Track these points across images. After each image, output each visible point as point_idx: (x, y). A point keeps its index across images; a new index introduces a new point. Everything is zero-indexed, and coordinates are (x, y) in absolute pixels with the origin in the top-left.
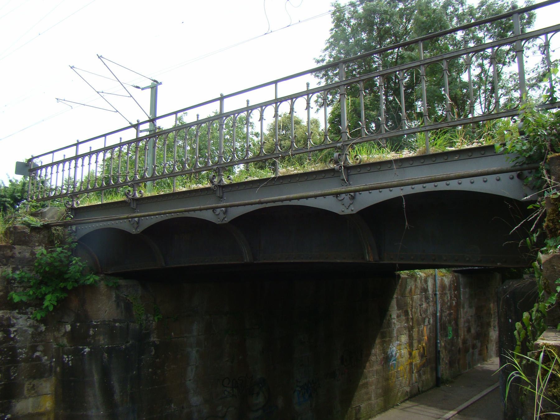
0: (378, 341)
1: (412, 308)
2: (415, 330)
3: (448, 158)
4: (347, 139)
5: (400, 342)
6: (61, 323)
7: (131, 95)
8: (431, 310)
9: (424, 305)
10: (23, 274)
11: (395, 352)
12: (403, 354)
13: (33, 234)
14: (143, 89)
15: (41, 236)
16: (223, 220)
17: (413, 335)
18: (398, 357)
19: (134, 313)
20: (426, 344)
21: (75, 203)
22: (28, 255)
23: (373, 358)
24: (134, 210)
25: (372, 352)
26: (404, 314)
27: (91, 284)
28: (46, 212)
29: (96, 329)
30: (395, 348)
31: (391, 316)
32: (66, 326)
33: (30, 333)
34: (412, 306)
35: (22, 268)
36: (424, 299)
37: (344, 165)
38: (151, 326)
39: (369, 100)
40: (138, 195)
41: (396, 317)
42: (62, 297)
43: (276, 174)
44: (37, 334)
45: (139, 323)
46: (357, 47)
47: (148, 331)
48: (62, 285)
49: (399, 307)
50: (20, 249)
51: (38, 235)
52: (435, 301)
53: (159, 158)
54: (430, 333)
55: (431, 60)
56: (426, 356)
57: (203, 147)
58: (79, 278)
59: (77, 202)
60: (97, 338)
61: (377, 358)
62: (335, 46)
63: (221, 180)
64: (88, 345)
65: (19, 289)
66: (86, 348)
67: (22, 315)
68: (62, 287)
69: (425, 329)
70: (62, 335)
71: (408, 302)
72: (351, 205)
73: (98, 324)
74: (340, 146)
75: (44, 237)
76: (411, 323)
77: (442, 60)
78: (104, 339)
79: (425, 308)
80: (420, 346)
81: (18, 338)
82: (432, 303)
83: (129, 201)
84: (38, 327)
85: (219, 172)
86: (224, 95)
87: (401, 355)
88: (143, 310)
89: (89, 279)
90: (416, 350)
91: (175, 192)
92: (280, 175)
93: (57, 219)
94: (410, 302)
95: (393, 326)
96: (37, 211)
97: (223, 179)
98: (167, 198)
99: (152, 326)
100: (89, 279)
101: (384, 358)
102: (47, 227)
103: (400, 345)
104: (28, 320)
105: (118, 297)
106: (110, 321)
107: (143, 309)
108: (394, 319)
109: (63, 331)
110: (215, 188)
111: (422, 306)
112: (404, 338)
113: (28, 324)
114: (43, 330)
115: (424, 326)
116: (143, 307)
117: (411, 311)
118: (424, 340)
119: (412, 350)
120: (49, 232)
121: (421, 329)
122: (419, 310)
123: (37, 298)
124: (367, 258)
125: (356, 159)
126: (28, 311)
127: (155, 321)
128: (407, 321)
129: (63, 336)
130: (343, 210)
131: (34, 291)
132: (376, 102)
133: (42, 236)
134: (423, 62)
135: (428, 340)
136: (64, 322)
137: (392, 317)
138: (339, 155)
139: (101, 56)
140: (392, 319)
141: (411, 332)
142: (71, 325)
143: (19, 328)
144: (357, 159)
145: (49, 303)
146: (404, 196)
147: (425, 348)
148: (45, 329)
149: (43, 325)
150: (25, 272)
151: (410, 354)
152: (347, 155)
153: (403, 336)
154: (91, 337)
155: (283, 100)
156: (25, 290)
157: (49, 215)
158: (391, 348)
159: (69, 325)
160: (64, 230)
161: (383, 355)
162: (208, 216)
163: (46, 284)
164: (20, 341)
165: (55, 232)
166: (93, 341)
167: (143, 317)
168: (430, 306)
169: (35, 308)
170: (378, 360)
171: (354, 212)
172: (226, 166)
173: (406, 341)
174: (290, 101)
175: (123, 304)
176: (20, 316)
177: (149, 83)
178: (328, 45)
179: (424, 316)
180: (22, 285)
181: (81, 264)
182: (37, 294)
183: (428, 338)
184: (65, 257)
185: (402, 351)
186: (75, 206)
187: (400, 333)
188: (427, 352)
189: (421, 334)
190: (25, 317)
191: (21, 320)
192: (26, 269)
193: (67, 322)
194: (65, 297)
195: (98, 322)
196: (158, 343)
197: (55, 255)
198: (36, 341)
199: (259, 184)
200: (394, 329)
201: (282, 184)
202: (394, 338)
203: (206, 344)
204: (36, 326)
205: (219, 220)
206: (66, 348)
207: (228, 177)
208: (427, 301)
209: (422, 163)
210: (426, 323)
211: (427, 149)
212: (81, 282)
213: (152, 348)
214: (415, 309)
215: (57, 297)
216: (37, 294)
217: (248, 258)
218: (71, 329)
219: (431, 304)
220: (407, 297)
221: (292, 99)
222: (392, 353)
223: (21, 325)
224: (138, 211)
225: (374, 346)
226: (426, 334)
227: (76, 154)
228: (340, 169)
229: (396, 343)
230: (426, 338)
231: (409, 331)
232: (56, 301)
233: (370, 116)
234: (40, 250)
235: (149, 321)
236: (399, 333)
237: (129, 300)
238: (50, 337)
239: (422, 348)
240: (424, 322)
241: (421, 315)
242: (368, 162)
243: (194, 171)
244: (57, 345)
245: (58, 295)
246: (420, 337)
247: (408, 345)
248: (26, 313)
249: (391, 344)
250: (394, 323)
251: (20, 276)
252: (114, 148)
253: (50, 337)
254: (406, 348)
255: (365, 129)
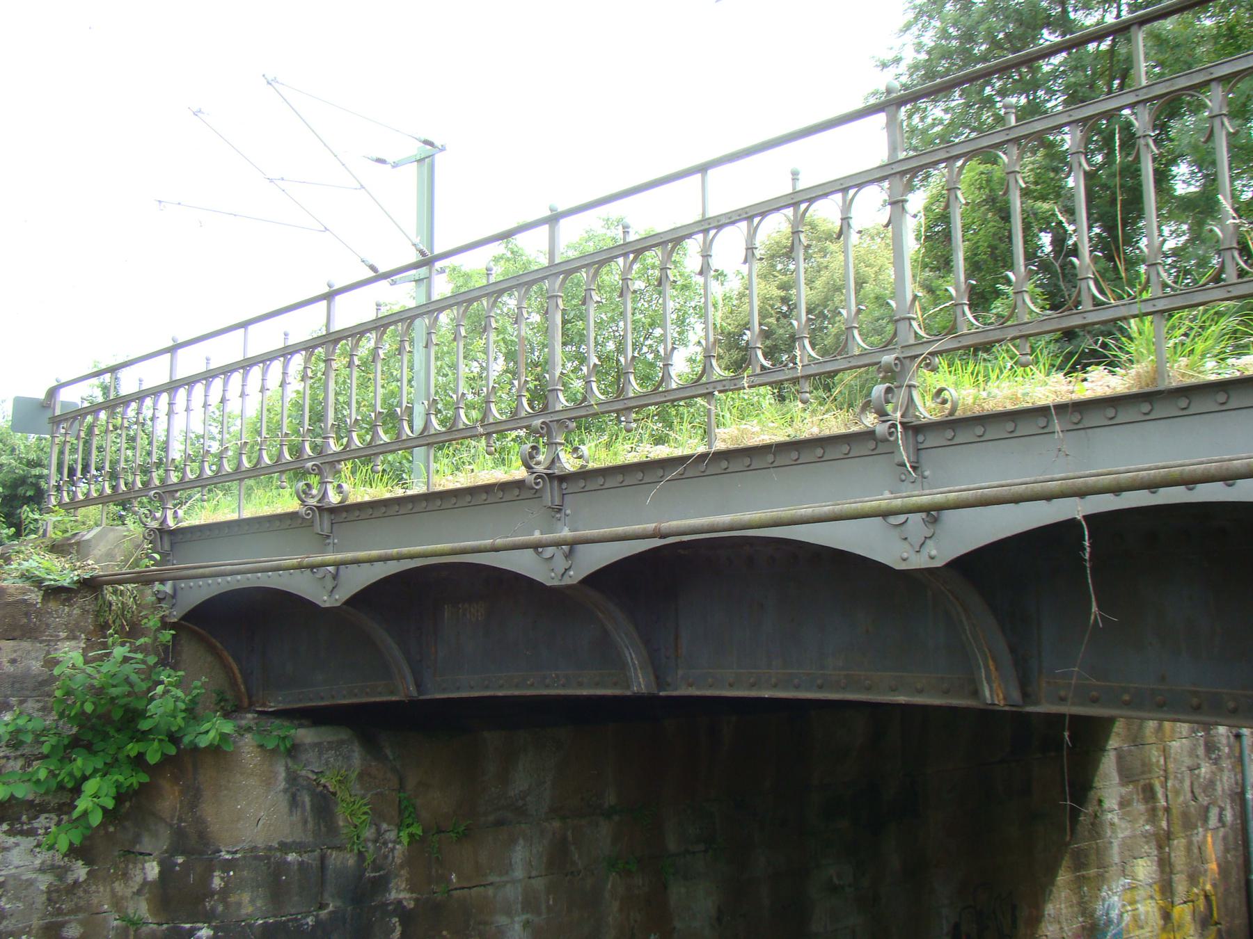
0: (1063, 877)
1: (1166, 778)
2: (1179, 843)
3: (1228, 398)
4: (912, 341)
5: (1133, 879)
6: (132, 855)
7: (361, 186)
8: (1226, 781)
9: (1205, 770)
10: (21, 722)
11: (1117, 912)
12: (1143, 917)
13: (52, 605)
14: (395, 165)
15: (75, 612)
16: (563, 575)
17: (1173, 859)
18: (1127, 925)
19: (341, 823)
20: (1214, 885)
21: (170, 514)
22: (36, 666)
23: (1051, 929)
24: (324, 540)
25: (1046, 912)
26: (1141, 796)
27: (211, 745)
28: (88, 541)
29: (232, 873)
30: (1116, 898)
31: (1100, 802)
32: (147, 865)
33: (43, 888)
34: (1165, 771)
35: (21, 702)
36: (1201, 751)
37: (905, 420)
38: (390, 858)
39: (1032, 170)
40: (334, 498)
41: (1116, 807)
42: (132, 784)
43: (710, 444)
44: (63, 891)
45: (356, 851)
46: (996, 16)
47: (382, 873)
48: (133, 749)
49: (1126, 776)
50: (15, 651)
51: (67, 609)
52: (1237, 754)
53: (448, 353)
54: (1227, 850)
55: (1172, 85)
56: (1217, 923)
57: (572, 315)
58: (180, 728)
59: (175, 512)
60: (232, 899)
61: (1061, 928)
62: (930, 17)
63: (555, 460)
64: (208, 918)
65: (12, 763)
66: (201, 929)
67: (19, 838)
68: (133, 754)
69: (1209, 840)
70: (135, 890)
71: (1154, 760)
72: (928, 541)
73: (237, 859)
74: (890, 364)
75: (85, 612)
76: (1164, 824)
77: (1206, 84)
78: (252, 901)
79: (1208, 776)
80: (1195, 890)
81: (8, 906)
82: (1228, 761)
83: (308, 514)
84: (65, 870)
85: (549, 434)
86: (560, 210)
87: (1136, 919)
88: (365, 813)
89: (207, 732)
90: (1185, 902)
91: (431, 490)
92: (719, 446)
93: (122, 561)
94: (1158, 761)
95: (1109, 833)
96: (69, 539)
97: (562, 455)
98: (410, 506)
99: (393, 857)
100: (207, 732)
101: (1083, 928)
102: (91, 585)
103: (1132, 888)
104: (38, 850)
105: (292, 778)
106: (270, 848)
107: (366, 809)
108: (1111, 811)
109: (139, 879)
110: (537, 484)
111: (1196, 772)
112: (1145, 869)
113: (38, 862)
114: (81, 879)
115: (1207, 830)
116: (365, 805)
117: (1165, 786)
118: (1209, 874)
119: (1172, 902)
120: (96, 598)
121: (1195, 839)
122: (1187, 784)
123: (61, 787)
124: (987, 693)
125: (939, 400)
126: (36, 825)
127: (400, 842)
128: (1153, 815)
129: (139, 893)
130: (905, 555)
131: (52, 768)
132: (1052, 175)
133: (77, 611)
134: (1146, 94)
135: (1219, 873)
136: (141, 854)
137: (1106, 805)
138: (889, 390)
139: (275, 80)
140: (1103, 811)
141: (1167, 850)
142: (161, 863)
143: (13, 875)
144: (944, 402)
145: (90, 805)
146: (1085, 517)
147: (1213, 898)
148: (88, 873)
149: (80, 863)
150: (29, 715)
151: (1166, 916)
152: (913, 389)
153: (1140, 861)
154: (216, 897)
155: (724, 221)
156: (30, 765)
157: (100, 549)
158: (1104, 900)
159: (155, 864)
160: (142, 592)
161: (1080, 919)
162: (523, 564)
163: (89, 748)
164: (11, 915)
165: (112, 598)
166: (220, 908)
167: (368, 833)
168: (1221, 770)
169: (58, 816)
170: (1065, 935)
171: (939, 563)
172: (570, 419)
173: (1152, 878)
174: (744, 225)
175: (307, 799)
176: (12, 840)
177: (416, 149)
178: (911, 15)
179: (1204, 800)
180: (19, 753)
181: (180, 693)
182: (59, 778)
183: (1219, 866)
184: (138, 672)
185: (1139, 906)
186: (171, 523)
187: (1130, 853)
188: (1218, 909)
189: (1197, 855)
190: (29, 842)
191: (15, 851)
192: (31, 705)
193: (150, 855)
194: (141, 784)
195: (236, 852)
196: (412, 904)
197: (107, 667)
198: (59, 912)
199: (660, 473)
200: (1111, 843)
201: (725, 472)
202: (1115, 868)
203: (551, 902)
204: (59, 867)
205: (553, 575)
206: (145, 930)
207: (576, 450)
208: (1213, 756)
209: (1145, 414)
210: (1213, 821)
211: (1159, 371)
212: (186, 740)
213: (395, 920)
214: (1177, 782)
215: (118, 785)
216: (59, 778)
217: (641, 680)
218: (160, 872)
219: (1226, 764)
220: (1147, 747)
221: (750, 219)
222: (1107, 914)
223: (17, 868)
224: (336, 541)
225: (1051, 891)
226: (1213, 856)
227: (171, 377)
228: (891, 434)
229: (1121, 883)
230: (1213, 866)
231: (1160, 847)
232: (114, 798)
233: (1035, 214)
234: (71, 654)
235: (385, 843)
236: (1127, 853)
237: (325, 786)
238: (101, 898)
239: (1202, 898)
240: (1205, 819)
241: (1195, 798)
242: (977, 411)
243: (481, 430)
244: (121, 919)
245: (121, 778)
246: (1195, 863)
247: (1156, 887)
248: (31, 832)
249: (1105, 887)
250: (1112, 824)
251: (11, 728)
252: (268, 360)
253: (101, 898)
254: (1152, 897)
255: (966, 309)
